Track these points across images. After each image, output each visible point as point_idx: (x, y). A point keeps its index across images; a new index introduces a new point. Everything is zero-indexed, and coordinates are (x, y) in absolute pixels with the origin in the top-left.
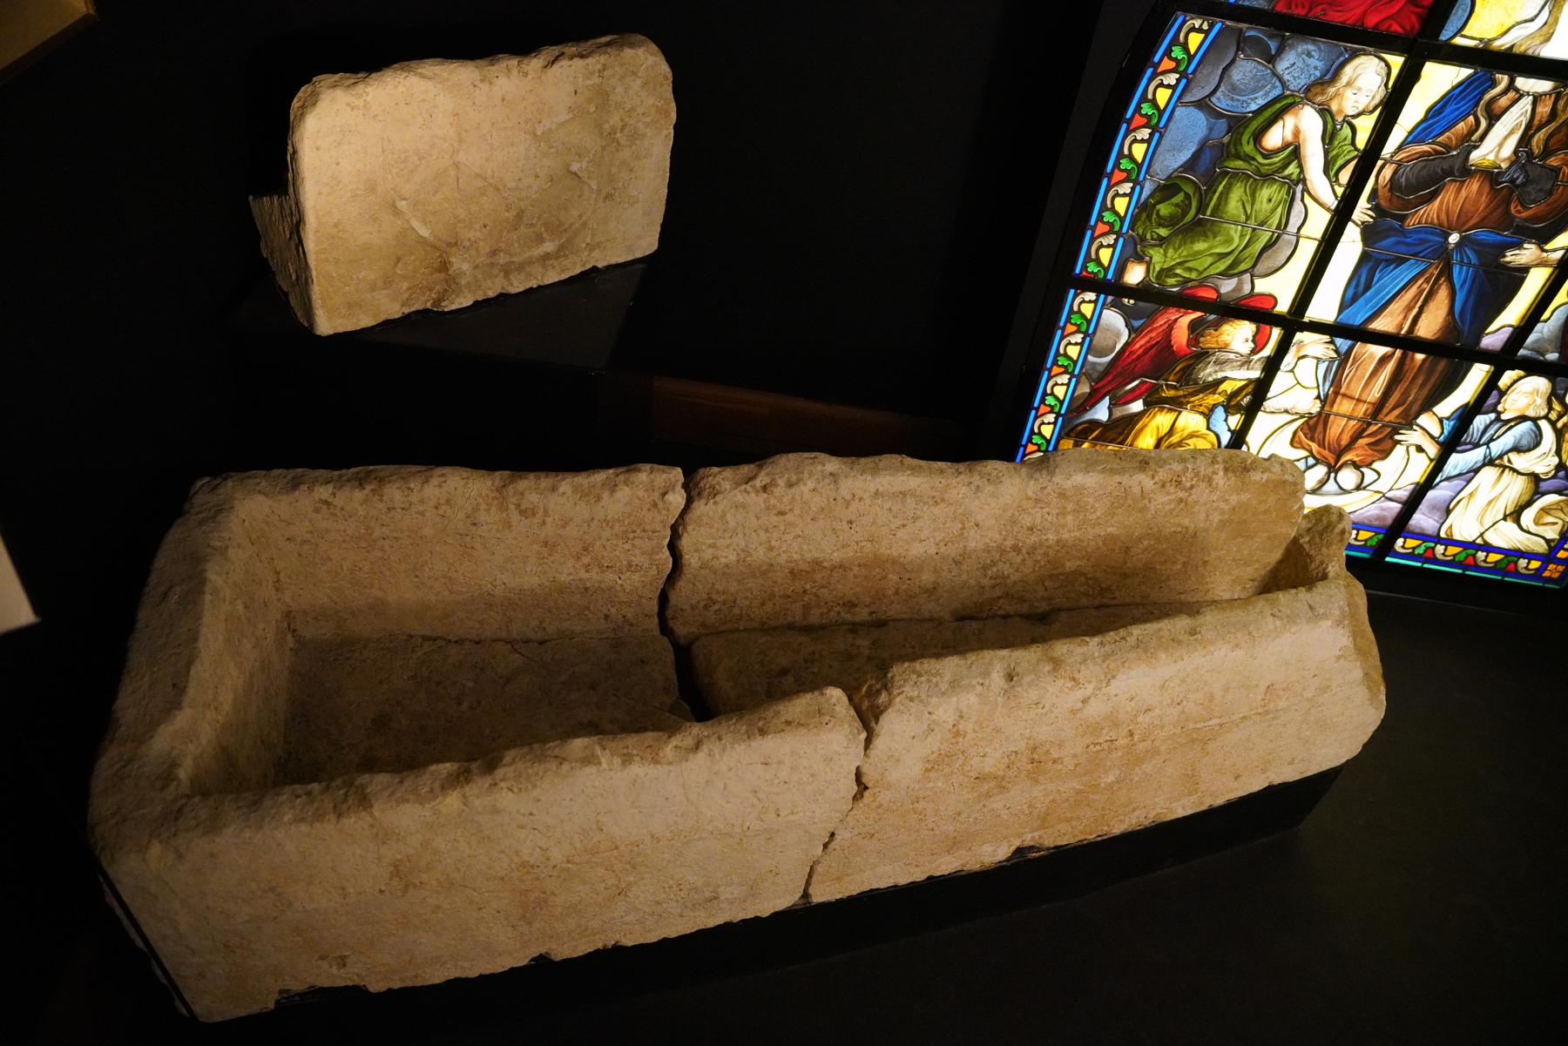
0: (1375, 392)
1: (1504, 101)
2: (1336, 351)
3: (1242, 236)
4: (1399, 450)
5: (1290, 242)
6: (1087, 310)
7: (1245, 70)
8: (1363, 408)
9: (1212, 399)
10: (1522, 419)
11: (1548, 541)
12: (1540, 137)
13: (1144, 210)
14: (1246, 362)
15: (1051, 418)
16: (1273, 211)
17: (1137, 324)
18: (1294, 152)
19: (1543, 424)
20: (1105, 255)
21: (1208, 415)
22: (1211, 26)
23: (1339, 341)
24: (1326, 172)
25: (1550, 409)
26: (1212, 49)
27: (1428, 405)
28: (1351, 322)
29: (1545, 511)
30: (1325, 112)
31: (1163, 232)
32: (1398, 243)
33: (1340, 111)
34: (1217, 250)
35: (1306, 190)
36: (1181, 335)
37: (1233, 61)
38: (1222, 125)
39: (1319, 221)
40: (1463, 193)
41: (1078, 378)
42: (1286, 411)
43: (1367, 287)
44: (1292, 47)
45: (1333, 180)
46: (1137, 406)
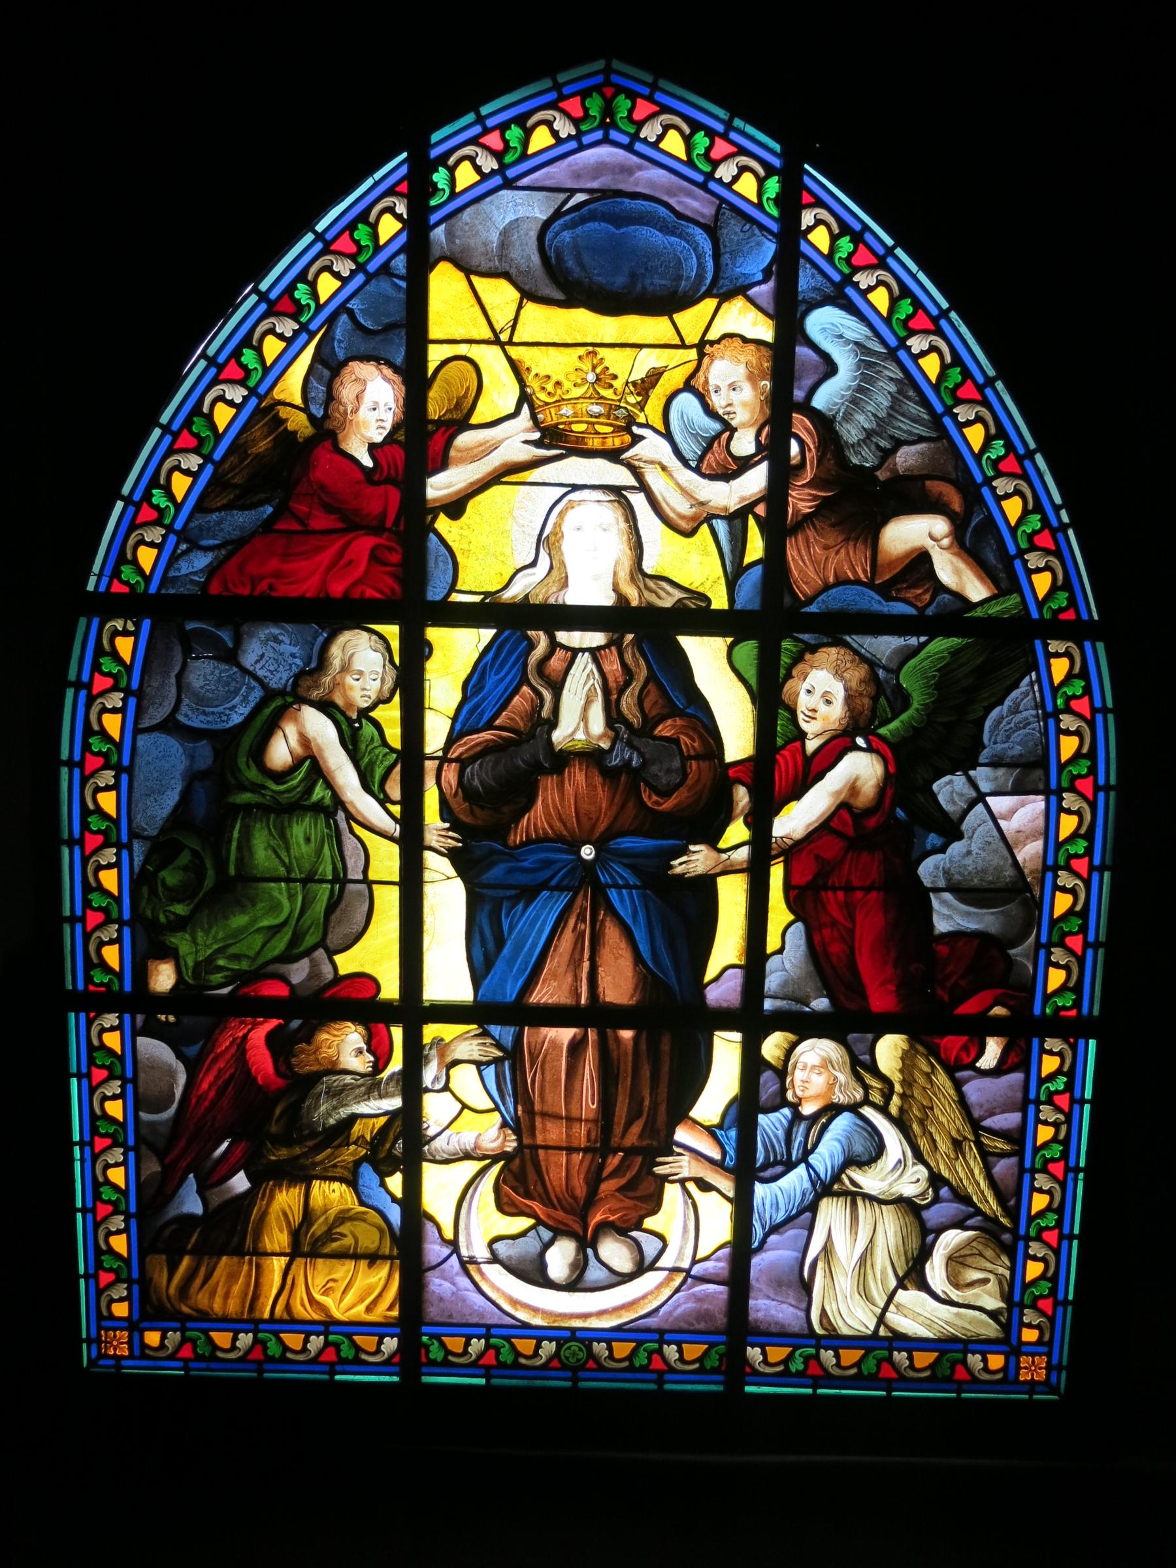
0: (588, 1102)
1: (556, 663)
2: (499, 1046)
3: (291, 897)
4: (672, 1192)
5: (360, 894)
6: (113, 1040)
7: (203, 673)
8: (581, 1133)
9: (351, 1153)
10: (832, 1110)
11: (993, 1314)
12: (628, 703)
13: (141, 882)
14: (372, 1085)
15: (118, 1222)
16: (319, 852)
17: (192, 1051)
18: (310, 763)
19: (867, 1111)
20: (111, 955)
21: (352, 1182)
22: (137, 625)
23: (495, 1030)
24: (366, 786)
25: (866, 1088)
26: (152, 656)
27: (680, 1111)
28: (499, 998)
29: (956, 1261)
30: (326, 707)
31: (180, 909)
32: (510, 871)
33: (350, 705)
34: (265, 923)
35: (350, 817)
36: (261, 1059)
37: (184, 665)
38: (204, 750)
39: (386, 860)
40: (569, 789)
41: (136, 1149)
42: (467, 1156)
43: (500, 943)
44: (251, 635)
45: (384, 801)
46: (240, 1182)
